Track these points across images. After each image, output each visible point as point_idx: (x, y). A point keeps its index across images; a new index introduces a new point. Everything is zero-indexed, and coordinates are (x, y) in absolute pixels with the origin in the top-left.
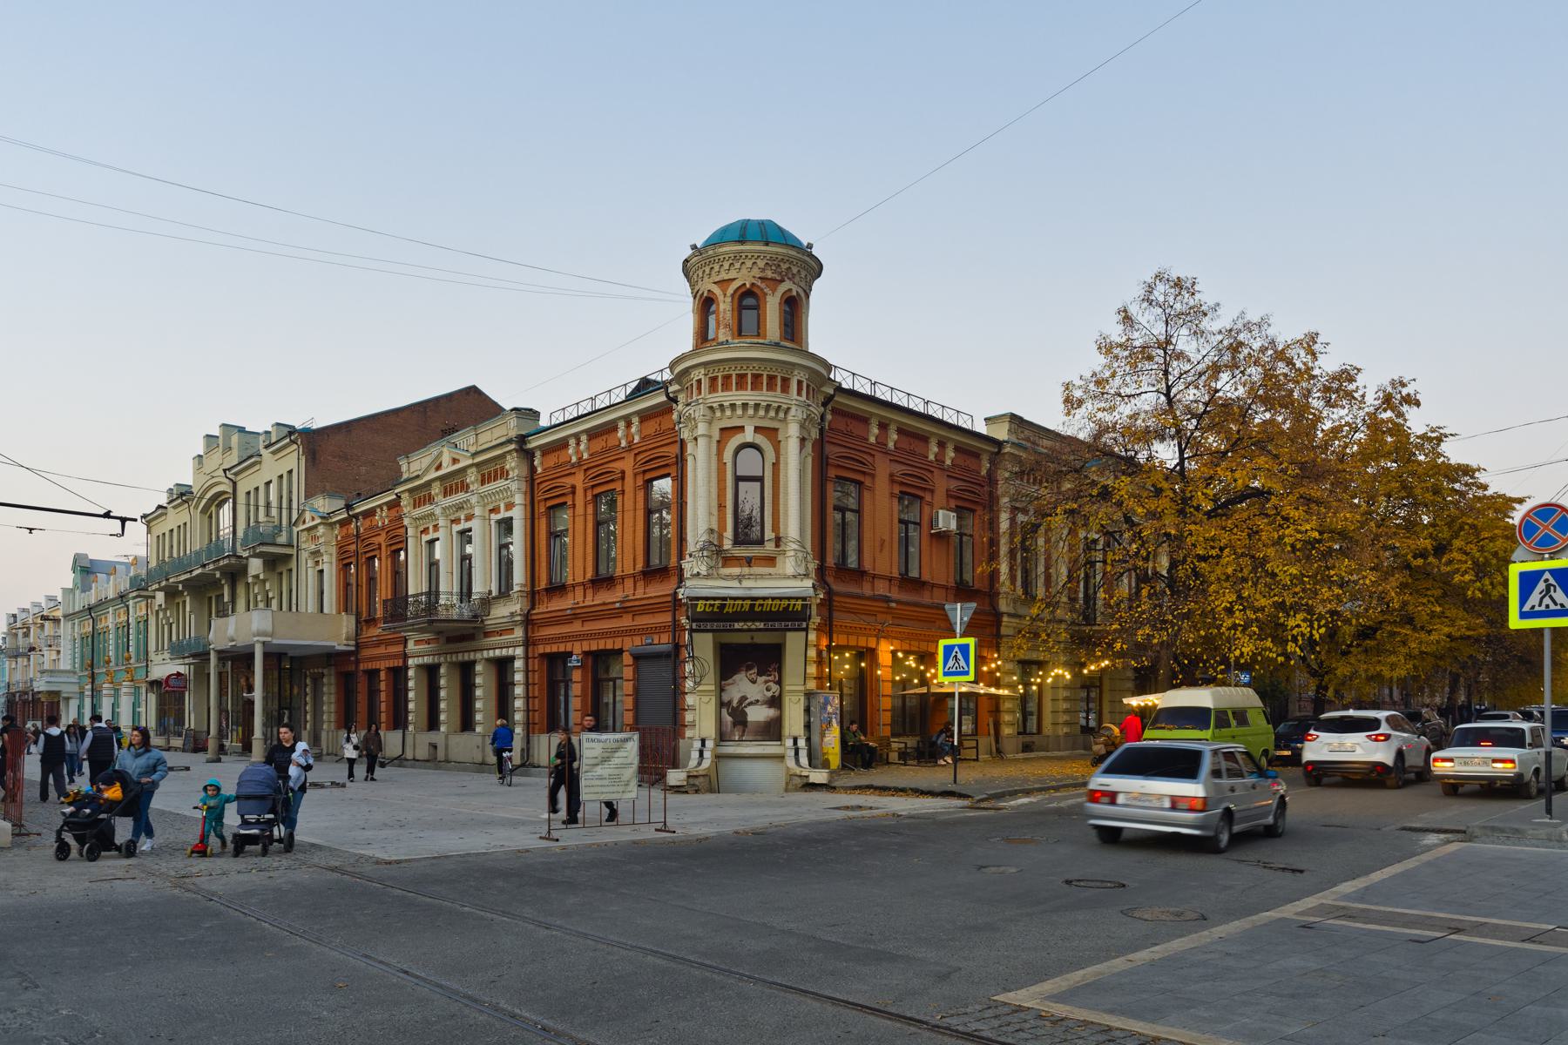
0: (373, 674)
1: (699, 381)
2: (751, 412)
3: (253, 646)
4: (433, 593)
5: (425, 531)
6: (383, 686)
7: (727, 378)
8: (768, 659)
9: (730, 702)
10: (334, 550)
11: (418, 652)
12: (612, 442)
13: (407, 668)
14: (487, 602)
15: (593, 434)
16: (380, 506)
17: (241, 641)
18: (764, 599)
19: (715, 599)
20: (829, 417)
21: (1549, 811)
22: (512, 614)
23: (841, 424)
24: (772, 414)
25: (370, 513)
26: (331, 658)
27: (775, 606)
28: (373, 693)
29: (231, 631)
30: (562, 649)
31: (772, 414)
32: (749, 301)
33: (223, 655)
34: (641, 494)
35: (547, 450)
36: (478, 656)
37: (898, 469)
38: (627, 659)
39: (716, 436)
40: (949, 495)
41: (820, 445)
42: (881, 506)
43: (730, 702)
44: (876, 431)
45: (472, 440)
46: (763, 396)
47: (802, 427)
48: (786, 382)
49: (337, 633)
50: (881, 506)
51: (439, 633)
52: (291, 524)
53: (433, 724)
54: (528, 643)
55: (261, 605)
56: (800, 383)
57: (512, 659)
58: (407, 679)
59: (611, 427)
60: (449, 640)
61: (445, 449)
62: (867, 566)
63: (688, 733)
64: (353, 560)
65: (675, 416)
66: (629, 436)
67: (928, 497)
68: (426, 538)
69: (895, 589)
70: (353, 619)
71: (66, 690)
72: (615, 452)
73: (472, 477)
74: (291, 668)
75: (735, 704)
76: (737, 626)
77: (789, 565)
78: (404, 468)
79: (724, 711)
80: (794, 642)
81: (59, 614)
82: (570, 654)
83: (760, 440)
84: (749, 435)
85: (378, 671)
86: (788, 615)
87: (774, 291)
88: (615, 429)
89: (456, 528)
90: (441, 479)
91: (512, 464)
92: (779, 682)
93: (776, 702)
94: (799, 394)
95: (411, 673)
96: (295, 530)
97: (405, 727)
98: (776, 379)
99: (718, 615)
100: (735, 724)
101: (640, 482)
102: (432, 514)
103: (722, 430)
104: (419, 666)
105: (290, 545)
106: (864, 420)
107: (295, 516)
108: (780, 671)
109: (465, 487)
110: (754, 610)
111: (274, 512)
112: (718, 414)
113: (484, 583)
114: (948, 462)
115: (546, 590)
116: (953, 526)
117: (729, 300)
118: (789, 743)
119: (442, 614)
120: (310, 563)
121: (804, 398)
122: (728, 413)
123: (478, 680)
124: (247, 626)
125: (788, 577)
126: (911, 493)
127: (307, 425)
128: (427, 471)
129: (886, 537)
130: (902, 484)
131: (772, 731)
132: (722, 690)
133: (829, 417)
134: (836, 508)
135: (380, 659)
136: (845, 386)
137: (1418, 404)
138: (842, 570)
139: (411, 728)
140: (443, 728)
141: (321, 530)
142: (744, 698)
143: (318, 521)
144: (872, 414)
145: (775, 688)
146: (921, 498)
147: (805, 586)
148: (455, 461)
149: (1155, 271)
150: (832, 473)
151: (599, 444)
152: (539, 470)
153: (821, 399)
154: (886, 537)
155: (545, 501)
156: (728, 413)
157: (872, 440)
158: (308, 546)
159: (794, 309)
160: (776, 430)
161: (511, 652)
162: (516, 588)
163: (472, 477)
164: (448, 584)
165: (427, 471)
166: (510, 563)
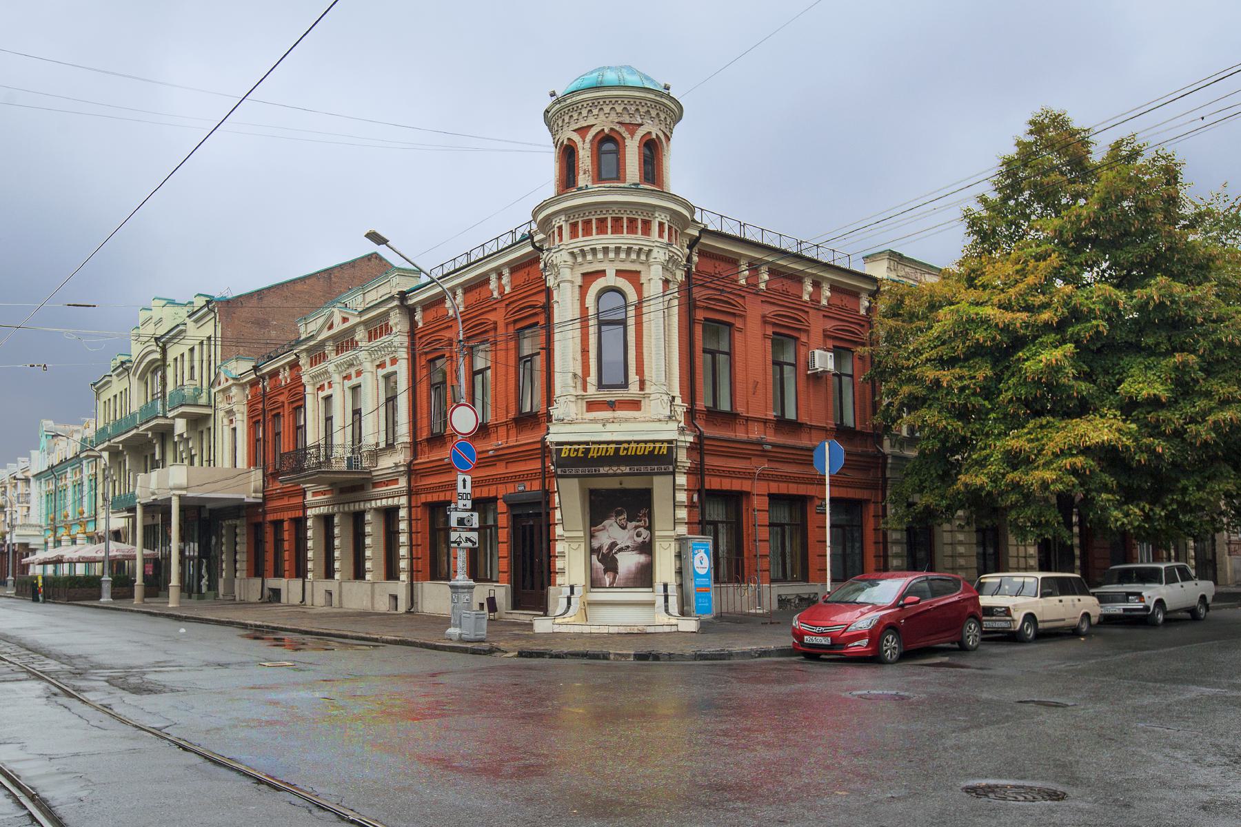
0: (278, 524)
1: (560, 228)
2: (612, 255)
4: (329, 445)
5: (321, 388)
6: (286, 536)
7: (588, 223)
8: (637, 505)
9: (600, 548)
10: (245, 409)
11: (316, 503)
12: (484, 295)
13: (306, 519)
14: (376, 454)
15: (468, 288)
16: (283, 366)
18: (629, 442)
19: (579, 443)
20: (695, 259)
22: (396, 465)
23: (709, 267)
24: (634, 256)
25: (274, 374)
26: (237, 509)
28: (278, 542)
29: (153, 485)
30: (442, 498)
31: (634, 256)
32: (609, 146)
33: (147, 507)
34: (512, 344)
35: (428, 305)
36: (368, 505)
37: (769, 310)
38: (502, 506)
39: (579, 281)
40: (826, 335)
41: (687, 287)
42: (752, 345)
43: (600, 548)
44: (810, 289)
45: (360, 299)
46: (625, 239)
47: (665, 268)
48: (647, 225)
49: (248, 486)
50: (752, 345)
51: (331, 485)
52: (211, 385)
53: (329, 573)
54: (411, 492)
55: (186, 462)
56: (661, 225)
57: (396, 509)
58: (306, 529)
59: (483, 281)
60: (343, 491)
61: (335, 310)
62: (740, 410)
63: (559, 579)
64: (261, 417)
65: (542, 265)
66: (501, 288)
67: (804, 339)
68: (322, 394)
69: (771, 431)
70: (259, 473)
71: (34, 542)
72: (489, 305)
73: (360, 335)
74: (204, 520)
76: (602, 470)
77: (656, 406)
78: (302, 329)
79: (594, 557)
80: (660, 486)
81: (29, 474)
83: (622, 283)
84: (611, 279)
85: (282, 522)
86: (657, 458)
87: (632, 134)
88: (487, 281)
89: (348, 384)
90: (333, 338)
91: (398, 322)
92: (650, 528)
93: (646, 548)
94: (661, 236)
95: (309, 523)
96: (213, 391)
97: (304, 577)
98: (637, 221)
99: (584, 460)
100: (606, 571)
101: (511, 329)
102: (326, 372)
103: (584, 275)
104: (317, 517)
105: (209, 406)
106: (733, 261)
107: (213, 377)
108: (650, 516)
109: (353, 344)
110: (619, 455)
111: (197, 375)
112: (580, 259)
113: (373, 433)
114: (824, 302)
115: (428, 440)
116: (830, 366)
117: (588, 145)
118: (659, 588)
119: (335, 467)
120: (226, 421)
121: (666, 240)
122: (600, 256)
123: (368, 529)
124: (171, 480)
125: (657, 419)
126: (785, 336)
127: (224, 294)
128: (320, 331)
129: (760, 379)
130: (775, 324)
131: (644, 577)
132: (592, 536)
133: (695, 259)
134: (705, 351)
135: (282, 511)
136: (711, 228)
138: (713, 415)
139: (310, 575)
140: (337, 576)
141: (234, 390)
142: (614, 544)
143: (231, 382)
144: (741, 255)
145: (645, 533)
146: (797, 339)
147: (669, 432)
148: (345, 320)
150: (700, 315)
151: (474, 296)
152: (420, 325)
153: (686, 242)
154: (760, 379)
155: (427, 353)
156: (589, 257)
157: (806, 297)
158: (222, 405)
159: (652, 150)
160: (639, 272)
161: (396, 501)
162: (400, 440)
163: (360, 335)
164: (341, 438)
165: (320, 331)
166: (746, 457)
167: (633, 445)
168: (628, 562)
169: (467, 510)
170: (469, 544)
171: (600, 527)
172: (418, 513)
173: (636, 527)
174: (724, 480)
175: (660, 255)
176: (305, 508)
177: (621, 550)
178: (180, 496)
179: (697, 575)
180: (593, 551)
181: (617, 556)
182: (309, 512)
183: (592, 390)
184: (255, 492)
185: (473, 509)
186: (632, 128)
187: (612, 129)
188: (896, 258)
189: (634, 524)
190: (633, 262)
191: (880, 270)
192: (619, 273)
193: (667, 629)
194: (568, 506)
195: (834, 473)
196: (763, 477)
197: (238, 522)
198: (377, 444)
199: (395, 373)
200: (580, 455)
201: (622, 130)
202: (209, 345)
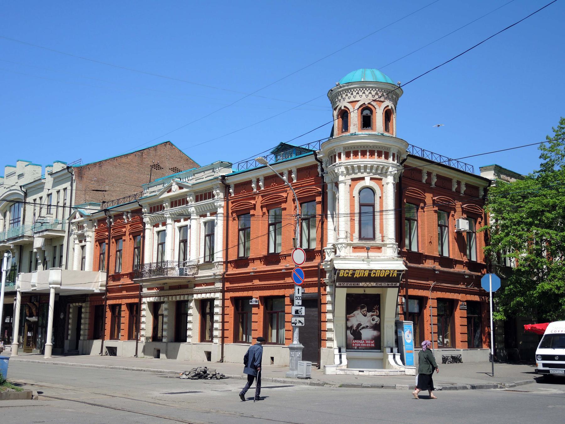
3: (49, 290)
17: (39, 288)
36: (190, 298)
43: (352, 327)
57: (212, 300)
70: (105, 275)
75: (354, 328)
76: (361, 284)
79: (349, 332)
82: (251, 298)
83: (373, 184)
84: (367, 182)
85: (120, 305)
87: (380, 106)
90: (171, 198)
93: (377, 327)
99: (350, 278)
103: (353, 180)
104: (149, 303)
110: (370, 277)
113: (196, 253)
142: (359, 325)
145: (377, 319)
149: (559, 120)
161: (212, 295)
168: (368, 334)
169: (299, 306)
170: (300, 325)
171: (352, 315)
172: (228, 303)
173: (372, 316)
176: (140, 297)
178: (55, 288)
179: (407, 343)
181: (361, 331)
182: (144, 300)
183: (356, 241)
184: (101, 286)
185: (302, 306)
188: (499, 170)
189: (371, 313)
191: (490, 175)
192: (372, 179)
193: (399, 373)
194: (334, 304)
195: (495, 291)
196: (435, 289)
197: (84, 305)
198: (199, 261)
199: (45, 183)
200: (349, 275)
202: (65, 195)
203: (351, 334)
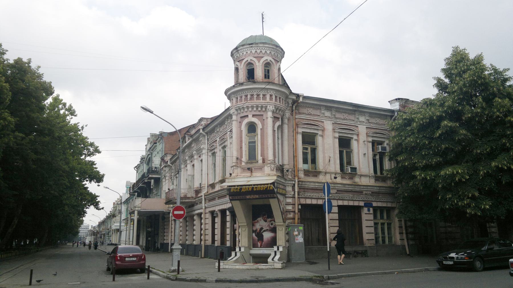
2: (250, 109)
21: (114, 280)
27: (262, 188)
43: (256, 230)
79: (254, 234)
83: (255, 120)
93: (274, 230)
100: (258, 240)
103: (241, 117)
122: (246, 110)
130: (373, 137)
137: (40, 67)
142: (262, 229)
156: (246, 110)
167: (269, 186)
171: (256, 221)
173: (271, 221)
174: (313, 200)
175: (271, 108)
177: (265, 231)
180: (253, 231)
186: (259, 58)
187: (251, 60)
189: (270, 219)
190: (259, 111)
200: (238, 191)
201: (254, 59)
203: (256, 236)
